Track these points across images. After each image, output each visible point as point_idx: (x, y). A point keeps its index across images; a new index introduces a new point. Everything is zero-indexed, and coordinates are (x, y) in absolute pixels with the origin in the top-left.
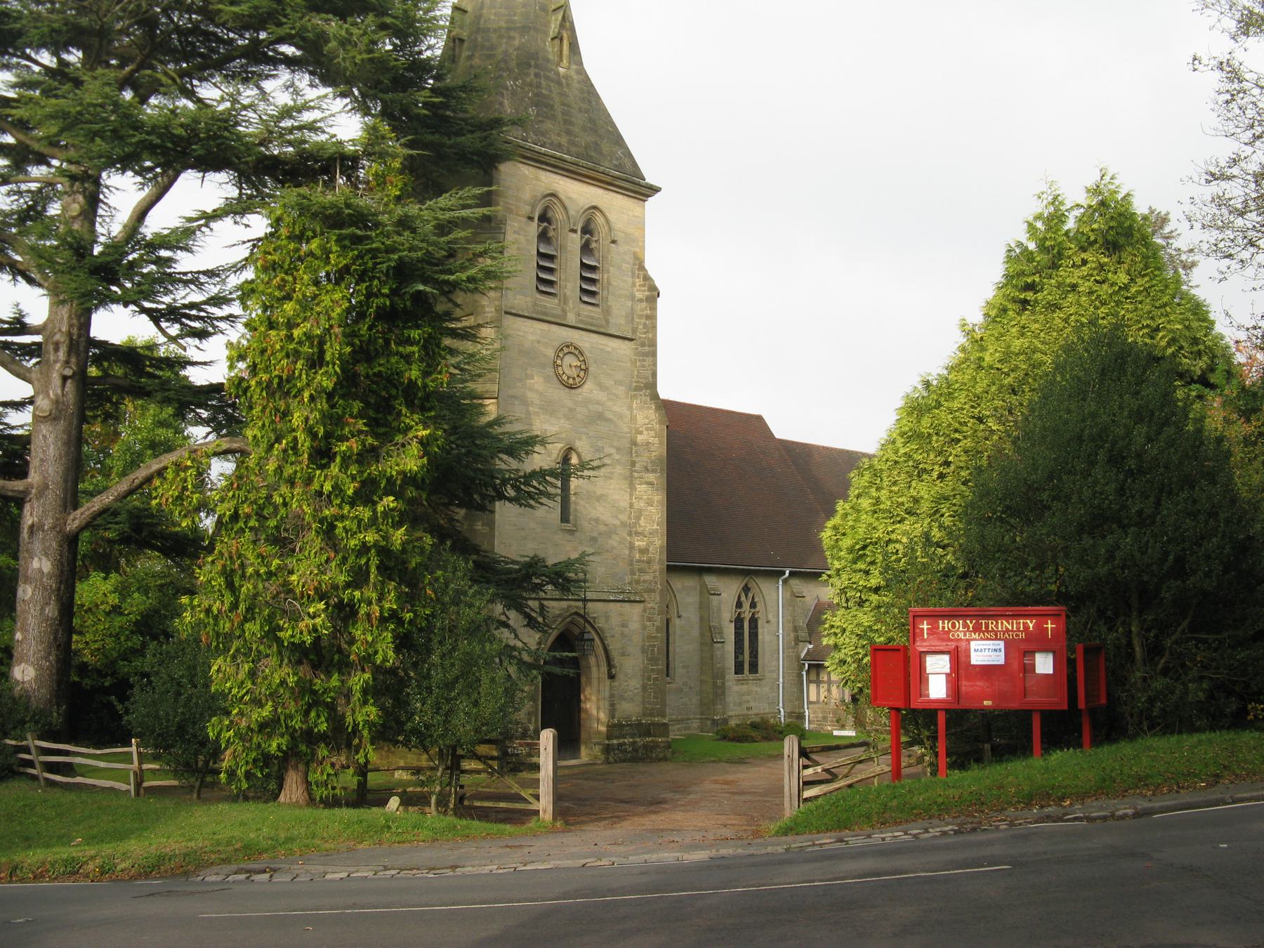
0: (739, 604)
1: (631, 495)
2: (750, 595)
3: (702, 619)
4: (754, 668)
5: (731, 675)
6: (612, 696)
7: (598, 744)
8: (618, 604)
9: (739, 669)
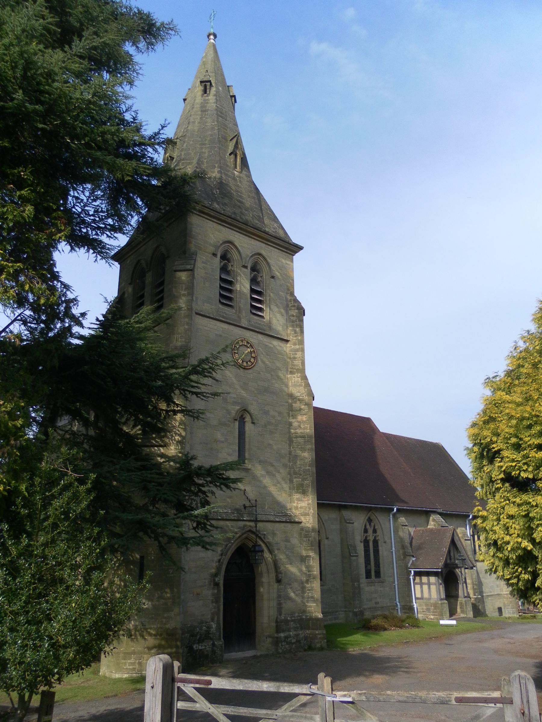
0: (366, 531)
1: (290, 445)
2: (372, 524)
3: (342, 540)
4: (378, 574)
5: (363, 579)
6: (279, 597)
7: (269, 636)
8: (282, 525)
9: (368, 575)
